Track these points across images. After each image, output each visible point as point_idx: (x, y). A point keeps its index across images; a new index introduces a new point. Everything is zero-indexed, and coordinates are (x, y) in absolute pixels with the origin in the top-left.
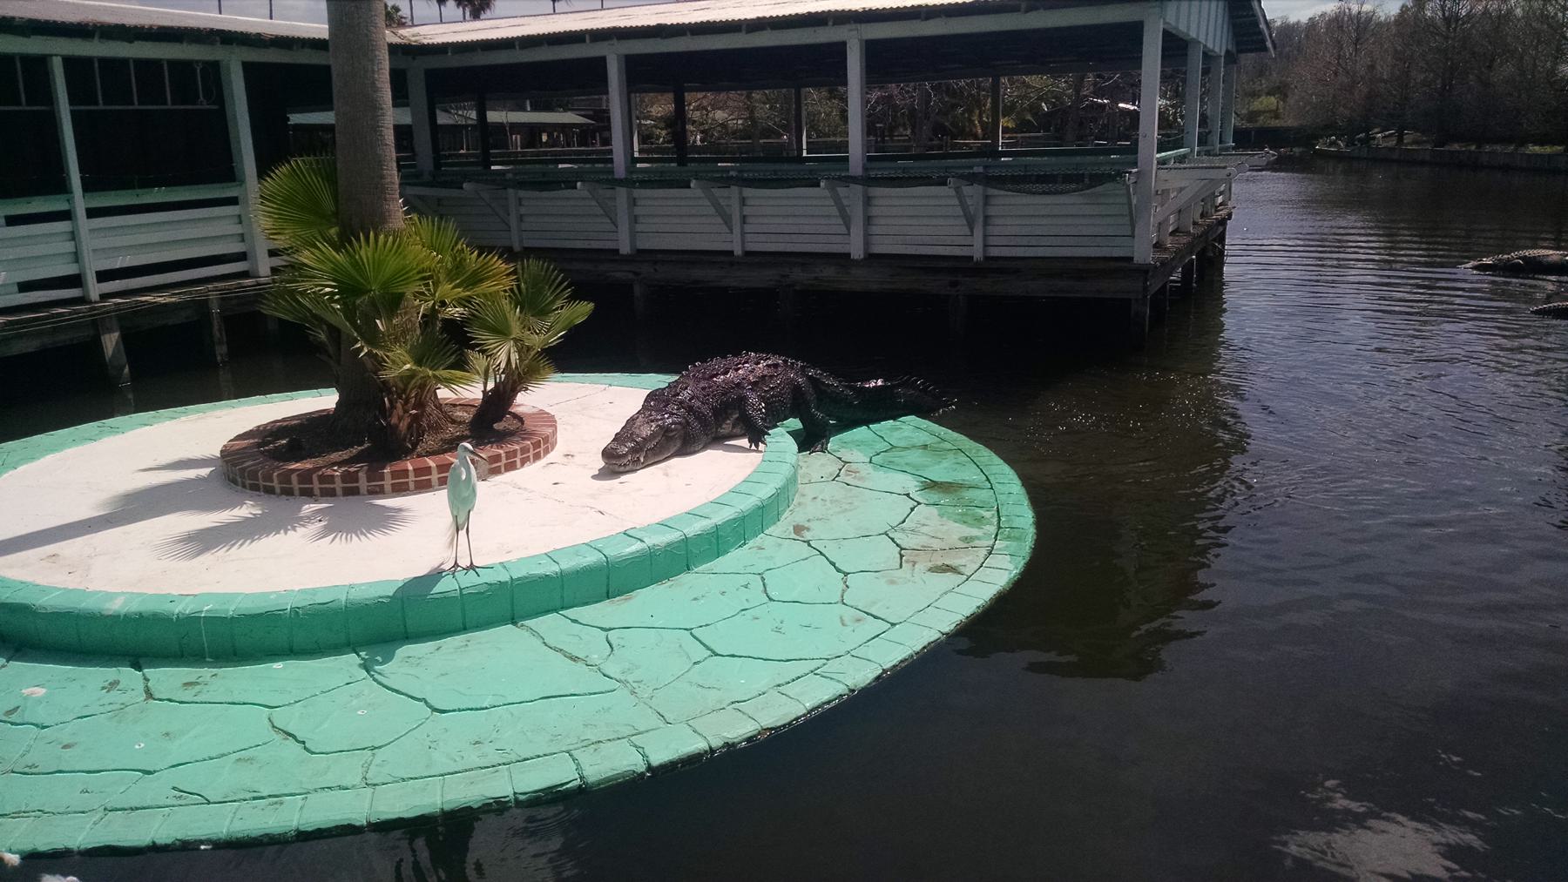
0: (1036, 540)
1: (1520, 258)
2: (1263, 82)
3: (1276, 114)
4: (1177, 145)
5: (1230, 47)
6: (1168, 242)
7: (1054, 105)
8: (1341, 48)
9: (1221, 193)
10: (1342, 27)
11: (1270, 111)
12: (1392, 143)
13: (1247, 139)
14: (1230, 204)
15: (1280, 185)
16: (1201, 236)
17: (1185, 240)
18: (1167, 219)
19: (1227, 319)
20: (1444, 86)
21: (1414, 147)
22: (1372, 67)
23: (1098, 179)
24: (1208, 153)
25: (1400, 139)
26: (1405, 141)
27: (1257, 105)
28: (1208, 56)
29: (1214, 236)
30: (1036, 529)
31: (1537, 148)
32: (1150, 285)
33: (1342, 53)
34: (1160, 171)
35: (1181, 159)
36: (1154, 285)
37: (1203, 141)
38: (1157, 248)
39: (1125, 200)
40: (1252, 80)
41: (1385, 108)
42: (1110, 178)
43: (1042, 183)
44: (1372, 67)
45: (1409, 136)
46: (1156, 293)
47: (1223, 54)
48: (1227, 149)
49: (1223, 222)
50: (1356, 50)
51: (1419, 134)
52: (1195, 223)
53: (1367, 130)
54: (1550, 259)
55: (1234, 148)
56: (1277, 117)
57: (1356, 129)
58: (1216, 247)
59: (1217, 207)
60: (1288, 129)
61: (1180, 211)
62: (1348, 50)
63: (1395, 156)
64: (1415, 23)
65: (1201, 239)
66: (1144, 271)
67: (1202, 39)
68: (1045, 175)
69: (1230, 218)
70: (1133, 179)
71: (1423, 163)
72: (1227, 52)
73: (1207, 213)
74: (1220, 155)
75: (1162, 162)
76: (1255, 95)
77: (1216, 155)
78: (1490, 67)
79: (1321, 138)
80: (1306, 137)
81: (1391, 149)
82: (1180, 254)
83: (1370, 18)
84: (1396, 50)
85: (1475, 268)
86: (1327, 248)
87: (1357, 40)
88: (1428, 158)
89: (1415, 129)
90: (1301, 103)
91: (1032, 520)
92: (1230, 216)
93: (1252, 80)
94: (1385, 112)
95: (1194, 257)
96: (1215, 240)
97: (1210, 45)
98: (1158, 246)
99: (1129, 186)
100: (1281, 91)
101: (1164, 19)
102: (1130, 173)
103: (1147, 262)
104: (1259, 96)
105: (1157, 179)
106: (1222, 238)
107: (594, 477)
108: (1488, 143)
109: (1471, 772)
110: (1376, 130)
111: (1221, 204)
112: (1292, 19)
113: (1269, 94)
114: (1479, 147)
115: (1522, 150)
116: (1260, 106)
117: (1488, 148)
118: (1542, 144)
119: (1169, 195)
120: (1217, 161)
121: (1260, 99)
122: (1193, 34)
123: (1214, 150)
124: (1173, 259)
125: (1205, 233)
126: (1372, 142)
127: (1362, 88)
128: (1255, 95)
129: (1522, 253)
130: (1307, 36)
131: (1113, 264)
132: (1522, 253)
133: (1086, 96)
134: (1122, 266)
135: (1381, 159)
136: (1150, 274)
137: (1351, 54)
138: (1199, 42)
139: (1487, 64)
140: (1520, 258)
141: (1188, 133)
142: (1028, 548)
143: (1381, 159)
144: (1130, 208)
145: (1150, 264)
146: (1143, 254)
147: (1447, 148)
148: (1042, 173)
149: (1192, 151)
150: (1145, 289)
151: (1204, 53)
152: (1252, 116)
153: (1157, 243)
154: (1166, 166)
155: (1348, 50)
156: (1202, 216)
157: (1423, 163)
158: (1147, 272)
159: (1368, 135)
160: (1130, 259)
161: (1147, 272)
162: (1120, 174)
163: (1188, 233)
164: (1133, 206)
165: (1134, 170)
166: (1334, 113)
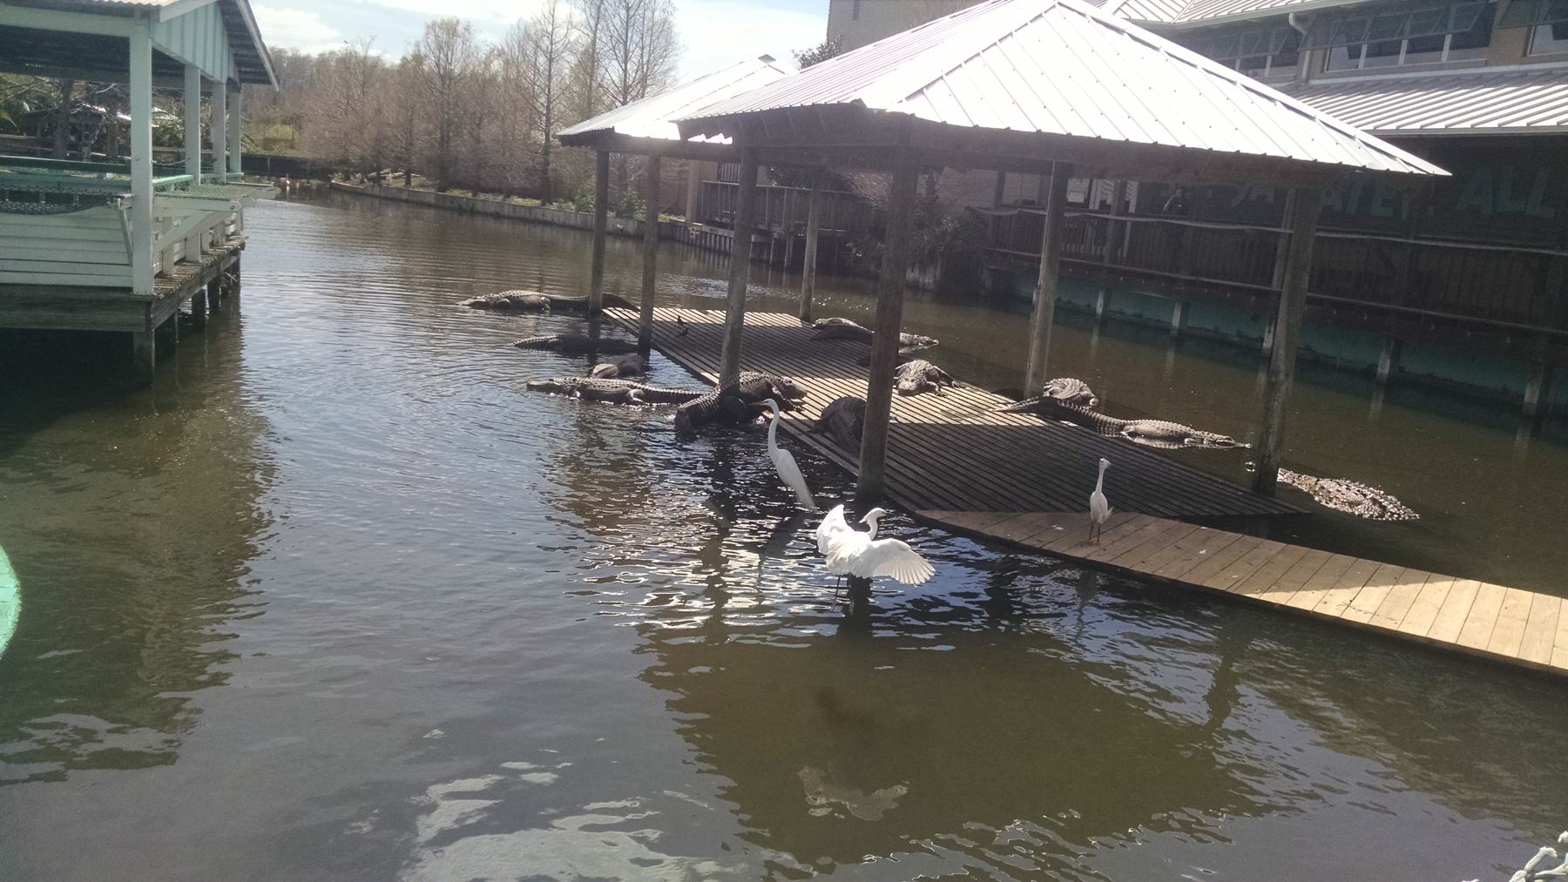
0: (21, 613)
1: (507, 297)
2: (277, 110)
3: (292, 145)
4: (178, 169)
5: (232, 76)
6: (174, 272)
7: (38, 107)
8: (349, 88)
9: (233, 222)
10: (349, 68)
11: (286, 141)
12: (401, 184)
13: (256, 166)
14: (244, 234)
15: (299, 216)
16: (211, 266)
17: (192, 270)
18: (170, 248)
19: (245, 354)
20: (442, 138)
21: (421, 190)
22: (379, 111)
23: (89, 201)
24: (214, 181)
25: (408, 182)
26: (413, 184)
27: (272, 132)
28: (206, 81)
29: (227, 266)
30: (21, 599)
31: (520, 200)
32: (155, 318)
33: (350, 93)
34: (158, 198)
35: (184, 186)
36: (159, 318)
37: (208, 164)
38: (160, 277)
39: (119, 226)
40: (267, 107)
41: (392, 151)
42: (100, 200)
43: (16, 201)
44: (379, 111)
45: (416, 180)
46: (161, 326)
47: (224, 81)
48: (236, 178)
49: (235, 252)
50: (364, 92)
51: (424, 179)
52: (204, 253)
53: (378, 170)
54: (529, 299)
55: (243, 178)
56: (292, 147)
57: (372, 166)
58: (229, 278)
59: (228, 236)
60: (304, 161)
61: (186, 240)
62: (357, 92)
63: (404, 196)
64: (415, 75)
65: (212, 269)
66: (146, 303)
67: (199, 64)
68: (19, 192)
69: (243, 248)
70: (127, 204)
71: (429, 206)
72: (229, 79)
73: (217, 242)
74: (227, 184)
75: (161, 189)
76: (269, 122)
77: (223, 184)
78: (479, 125)
79: (337, 172)
80: (322, 171)
81: (400, 190)
82: (186, 285)
83: (376, 63)
84: (399, 98)
85: (473, 305)
86: (347, 285)
87: (364, 83)
88: (433, 201)
89: (421, 172)
90: (315, 137)
91: (15, 590)
92: (243, 246)
93: (267, 107)
94: (393, 155)
95: (205, 287)
96: (227, 270)
97: (209, 71)
98: (161, 276)
99: (121, 212)
100: (295, 121)
101: (152, 39)
102: (122, 198)
103: (148, 293)
104: (274, 124)
105: (154, 206)
106: (235, 269)
107: (760, 58)
108: (483, 192)
109: (569, 764)
110: (386, 171)
111: (233, 234)
112: (303, 52)
113: (284, 122)
114: (475, 195)
115: (508, 201)
116: (275, 134)
117: (482, 196)
118: (524, 196)
119: (171, 223)
120: (222, 191)
121: (275, 127)
122: (188, 58)
123: (220, 178)
124: (180, 290)
125: (215, 264)
126: (383, 181)
127: (371, 130)
128: (269, 122)
129: (509, 293)
130: (318, 70)
131: (93, 295)
132: (509, 293)
133: (76, 102)
134: (121, 298)
135: (391, 199)
136: (153, 306)
137: (359, 96)
138: (197, 67)
139: (477, 122)
140: (507, 297)
141: (189, 159)
142: (10, 623)
143: (391, 199)
144: (125, 234)
145: (153, 296)
146: (145, 285)
147: (448, 193)
148: (16, 189)
149: (196, 178)
150: (149, 321)
151: (202, 76)
152: (268, 143)
153: (161, 272)
154: (164, 193)
155: (357, 92)
156: (212, 244)
157: (429, 206)
158: (149, 304)
159: (379, 174)
160: (129, 290)
161: (149, 304)
162: (113, 198)
163: (195, 263)
164: (129, 233)
165: (126, 195)
166: (347, 150)
